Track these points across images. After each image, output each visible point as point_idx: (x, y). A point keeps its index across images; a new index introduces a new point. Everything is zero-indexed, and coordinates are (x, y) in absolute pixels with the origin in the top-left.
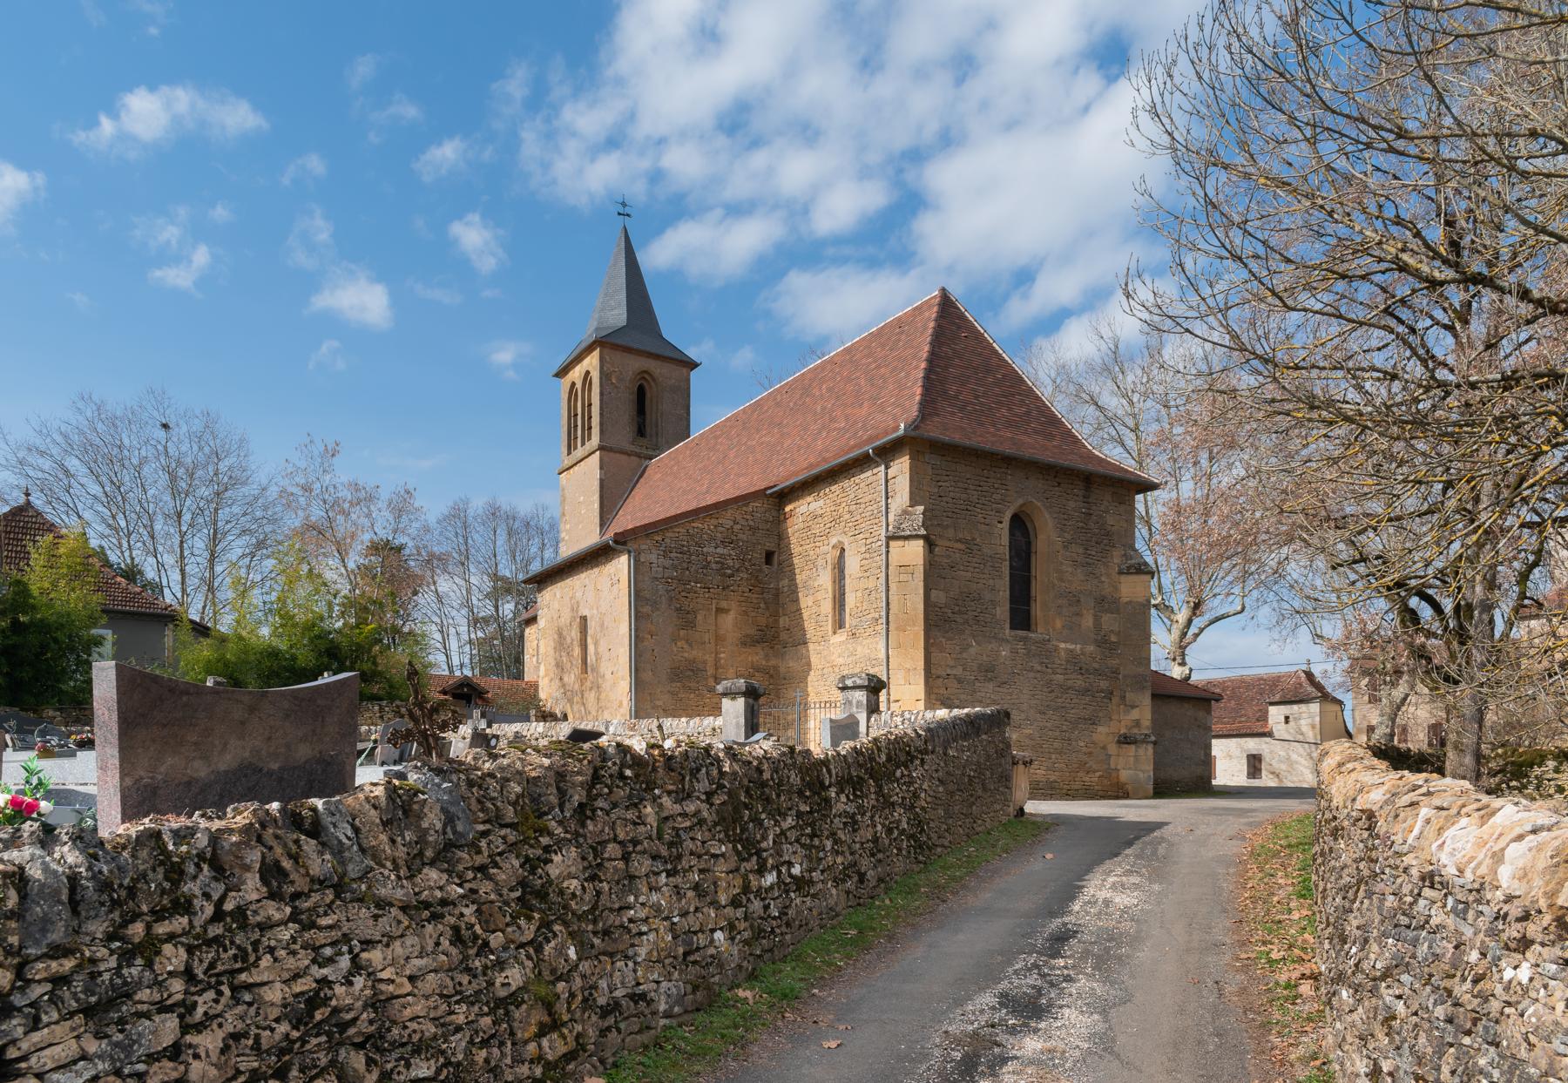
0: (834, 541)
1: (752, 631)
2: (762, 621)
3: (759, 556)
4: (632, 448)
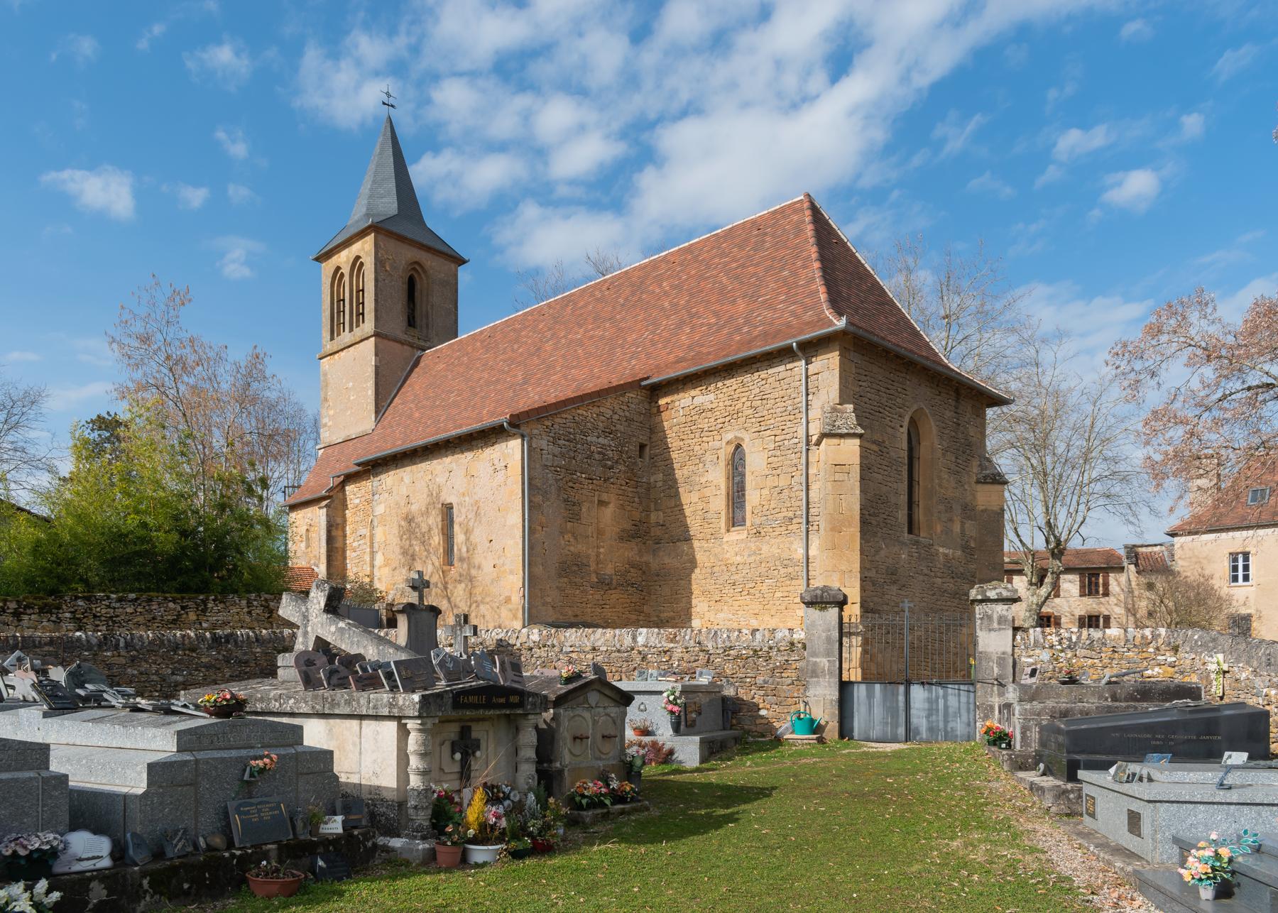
0: (730, 436)
1: (628, 526)
2: (637, 515)
3: (633, 448)
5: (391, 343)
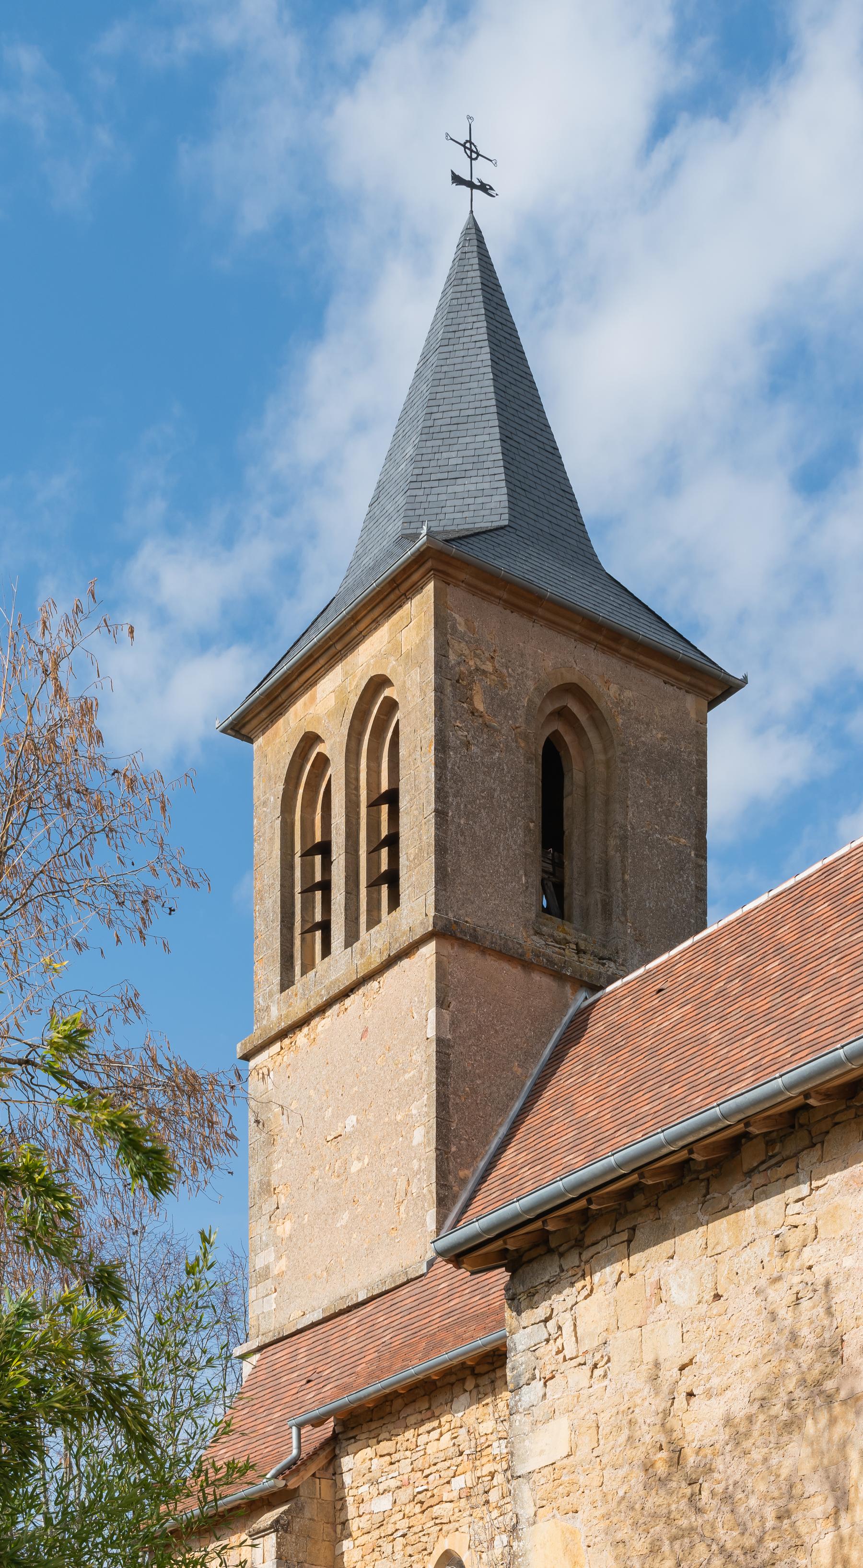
4: (532, 943)
5: (491, 964)
